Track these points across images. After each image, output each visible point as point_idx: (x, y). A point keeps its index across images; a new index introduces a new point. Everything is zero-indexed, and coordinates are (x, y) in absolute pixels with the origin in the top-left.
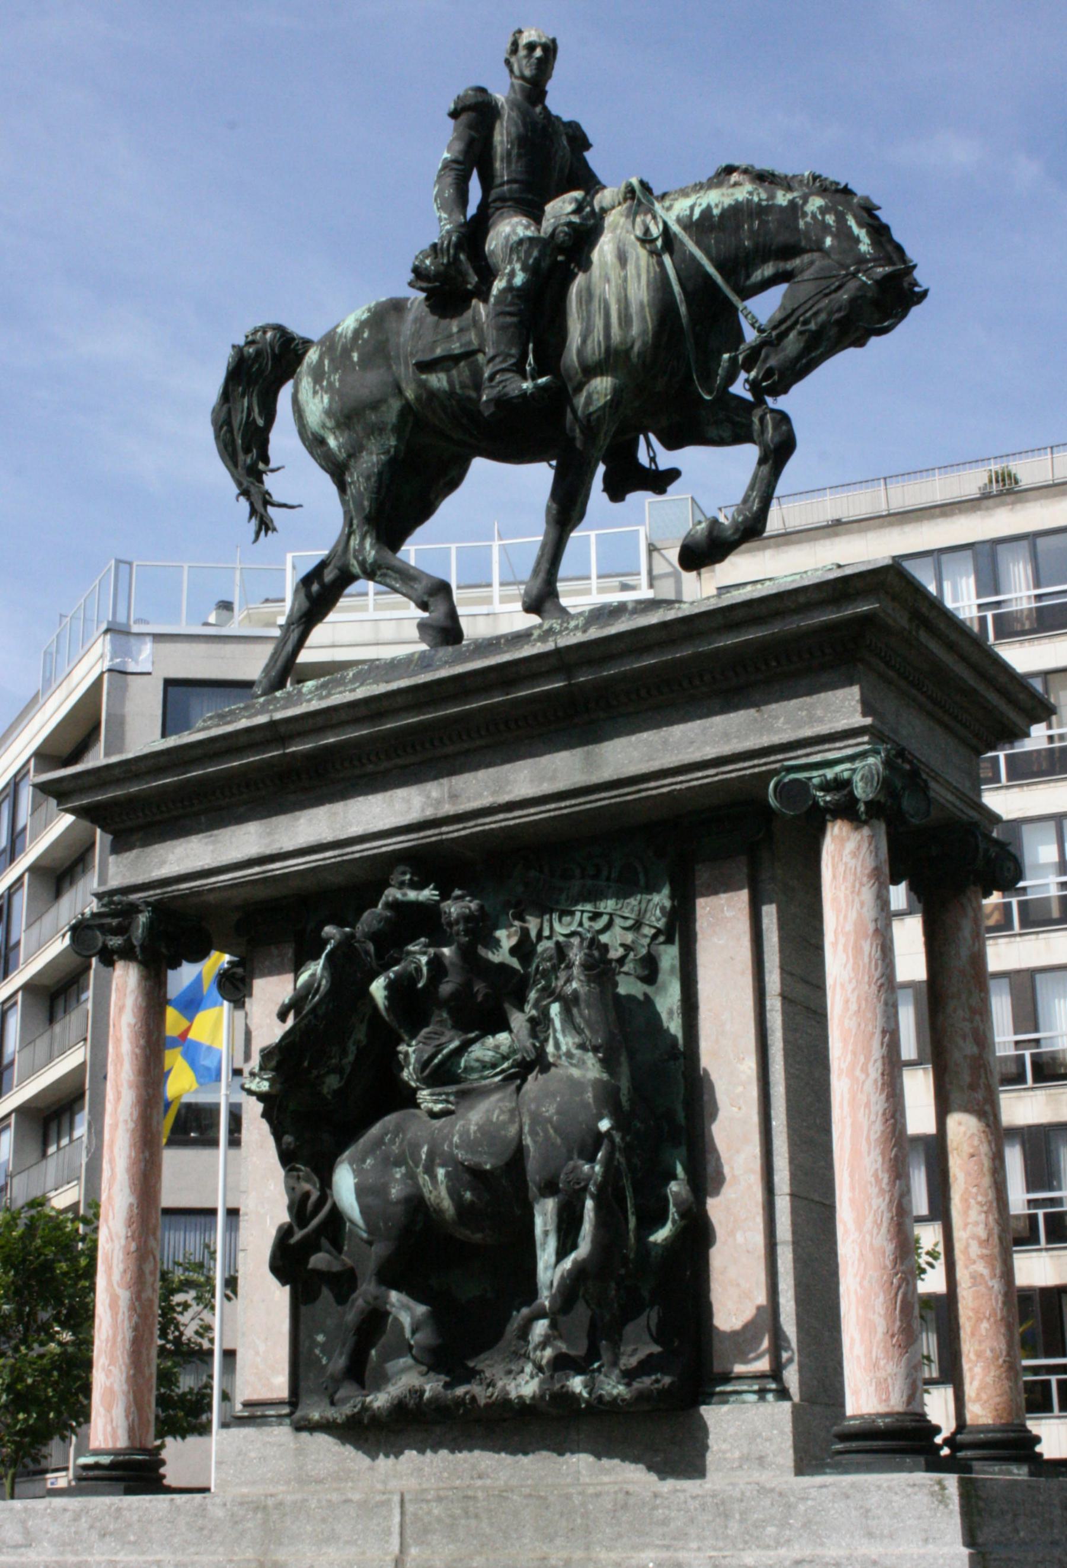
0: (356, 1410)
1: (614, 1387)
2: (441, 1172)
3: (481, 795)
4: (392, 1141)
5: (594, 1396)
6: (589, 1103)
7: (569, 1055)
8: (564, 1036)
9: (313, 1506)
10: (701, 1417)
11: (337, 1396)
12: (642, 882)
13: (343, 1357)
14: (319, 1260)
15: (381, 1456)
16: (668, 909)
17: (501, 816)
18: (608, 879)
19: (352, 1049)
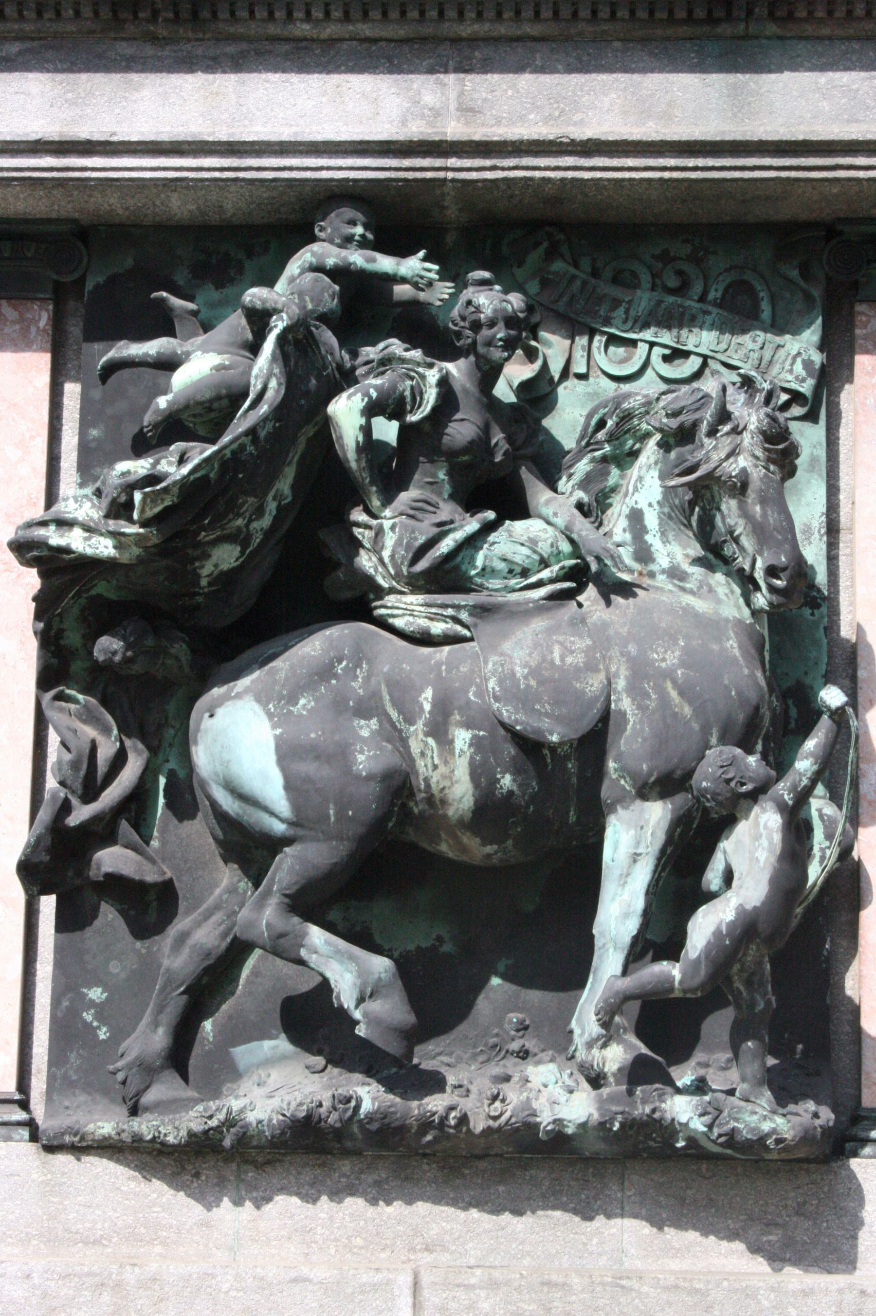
0: (214, 1123)
1: (765, 1118)
2: (462, 738)
3: (522, 118)
4: (351, 673)
5: (716, 1131)
6: (735, 658)
7: (675, 573)
8: (665, 541)
9: (225, 1287)
10: (852, 1176)
11: (149, 1097)
12: (766, 314)
13: (161, 1031)
14: (111, 859)
15: (226, 1202)
16: (817, 366)
17: (569, 161)
18: (702, 299)
19: (272, 507)
